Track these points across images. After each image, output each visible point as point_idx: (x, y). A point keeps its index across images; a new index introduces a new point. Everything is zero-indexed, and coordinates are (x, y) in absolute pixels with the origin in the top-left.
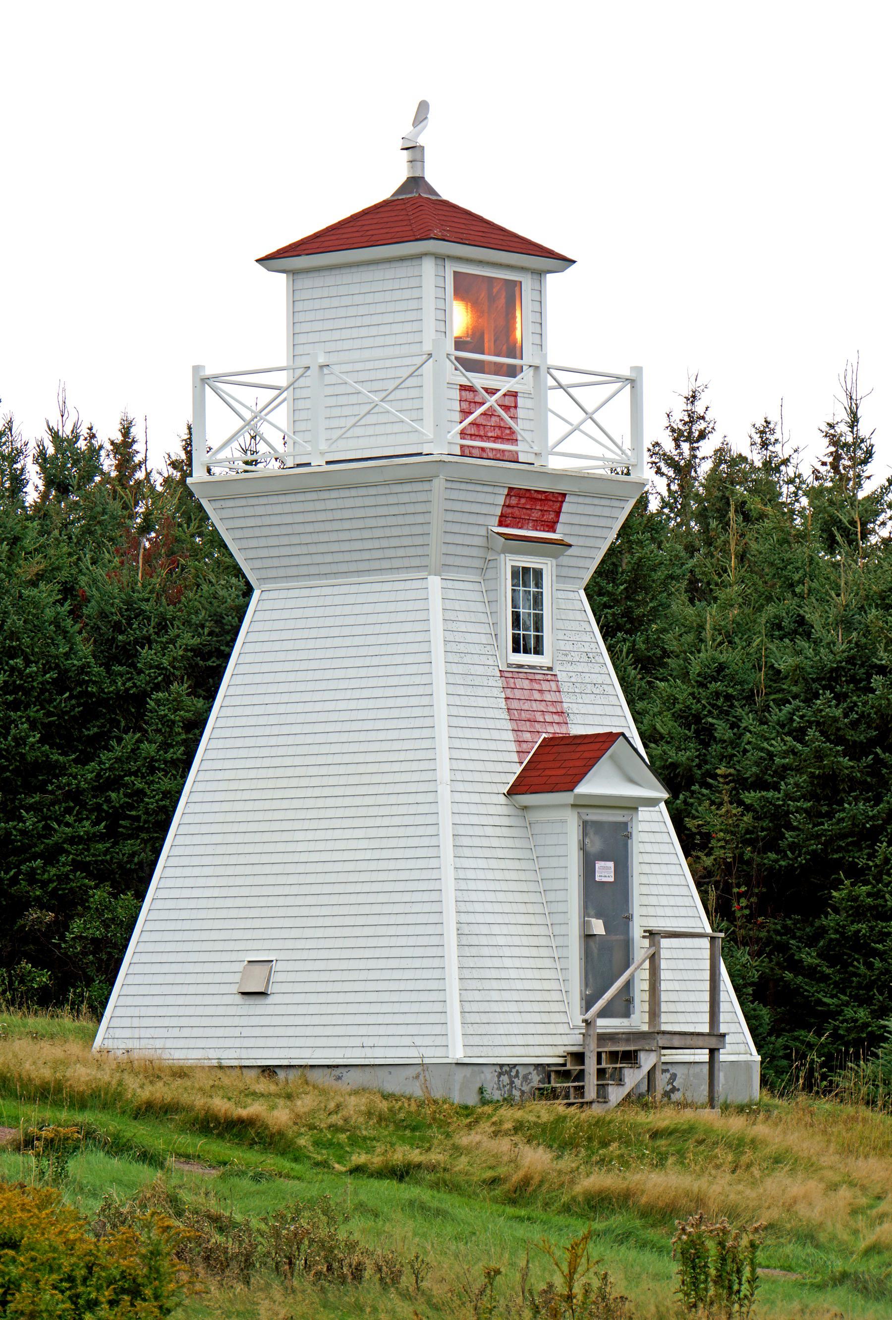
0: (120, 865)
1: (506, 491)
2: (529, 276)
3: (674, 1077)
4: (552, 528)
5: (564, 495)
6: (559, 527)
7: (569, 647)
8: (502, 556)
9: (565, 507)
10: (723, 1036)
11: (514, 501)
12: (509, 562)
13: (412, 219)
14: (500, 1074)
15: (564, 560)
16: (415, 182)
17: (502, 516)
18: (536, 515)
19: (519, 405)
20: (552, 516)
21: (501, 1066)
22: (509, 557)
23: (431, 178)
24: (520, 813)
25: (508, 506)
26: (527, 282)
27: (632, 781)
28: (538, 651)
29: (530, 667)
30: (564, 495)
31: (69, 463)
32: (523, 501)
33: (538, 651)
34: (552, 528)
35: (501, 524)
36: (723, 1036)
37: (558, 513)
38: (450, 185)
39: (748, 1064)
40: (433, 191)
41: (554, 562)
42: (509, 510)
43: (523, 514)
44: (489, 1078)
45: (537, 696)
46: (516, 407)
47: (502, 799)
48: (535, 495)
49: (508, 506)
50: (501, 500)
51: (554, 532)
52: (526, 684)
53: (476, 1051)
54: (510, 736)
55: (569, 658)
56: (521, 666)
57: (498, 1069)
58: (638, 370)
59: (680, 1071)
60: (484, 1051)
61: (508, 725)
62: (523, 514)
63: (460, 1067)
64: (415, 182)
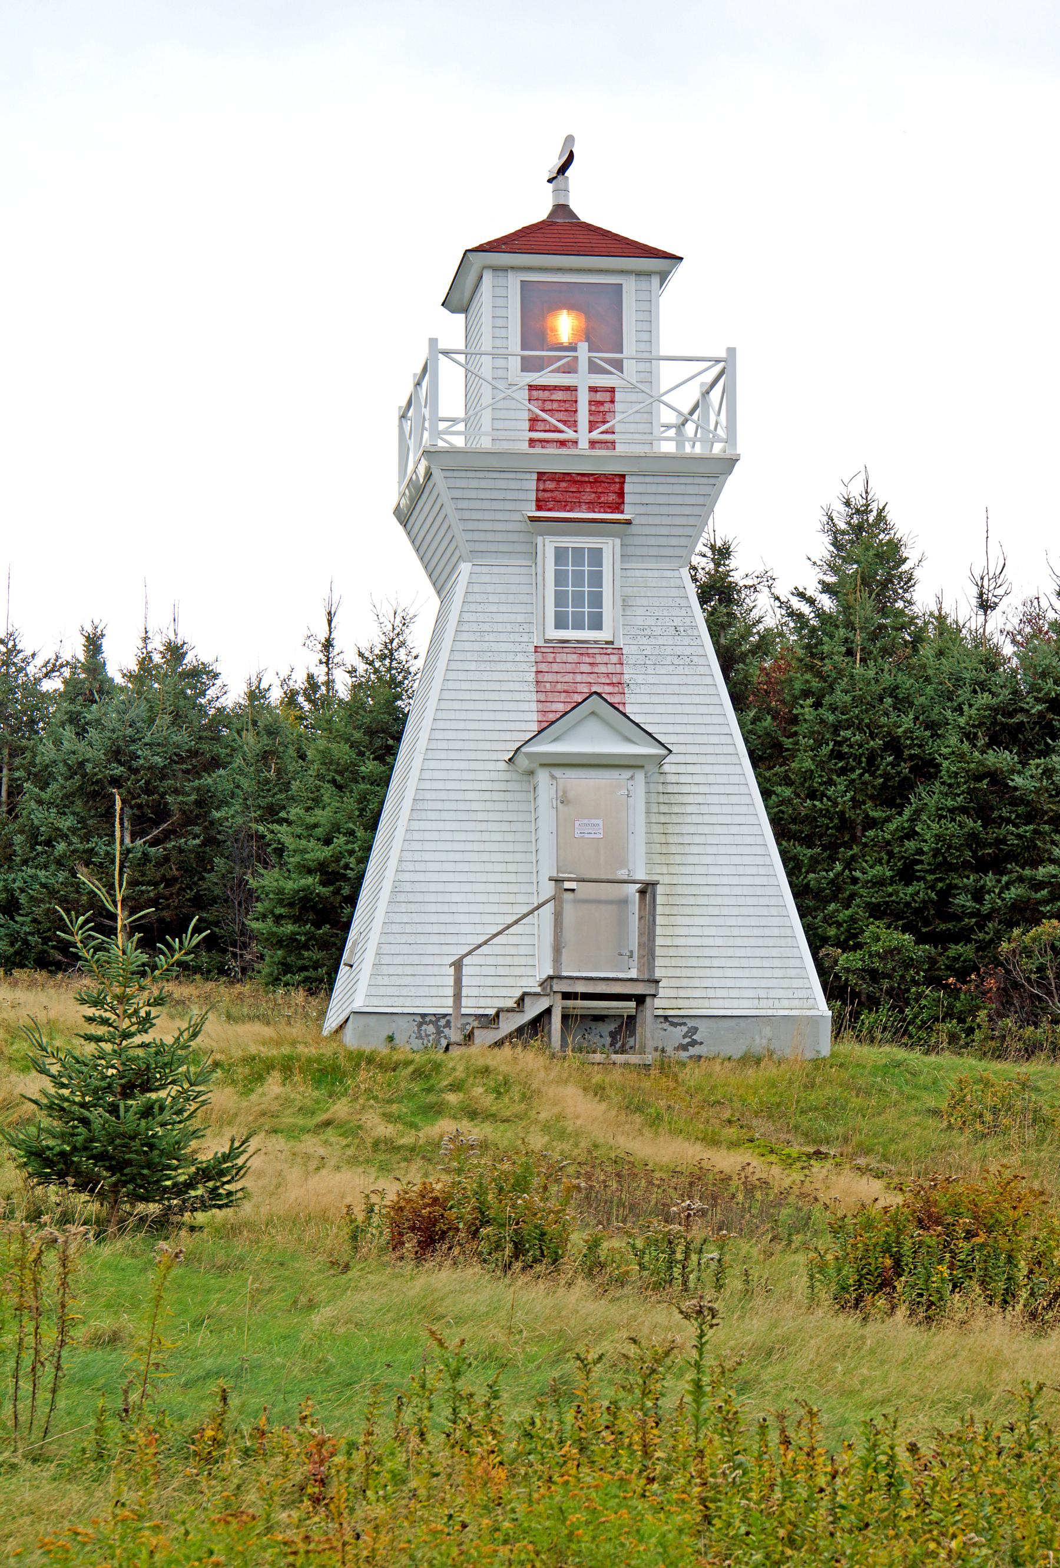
0: (908, 905)
1: (535, 476)
2: (633, 278)
3: (694, 1030)
4: (618, 507)
5: (623, 476)
6: (627, 508)
7: (651, 621)
8: (540, 539)
9: (627, 488)
10: (657, 982)
11: (550, 485)
12: (548, 546)
13: (561, 235)
14: (420, 1025)
15: (629, 540)
16: (561, 209)
17: (538, 500)
18: (587, 497)
19: (617, 398)
20: (612, 497)
21: (423, 1016)
22: (548, 539)
23: (574, 207)
24: (525, 778)
25: (544, 491)
26: (630, 286)
27: (628, 740)
28: (597, 624)
29: (578, 642)
30: (623, 476)
31: (895, 546)
32: (563, 484)
33: (597, 624)
34: (618, 507)
35: (539, 508)
36: (657, 982)
37: (621, 494)
38: (589, 211)
39: (813, 1021)
40: (573, 215)
41: (618, 541)
42: (547, 495)
43: (568, 497)
44: (404, 1031)
45: (586, 668)
46: (612, 401)
47: (503, 766)
48: (579, 478)
49: (544, 491)
50: (533, 485)
51: (622, 512)
52: (573, 658)
53: (375, 1001)
54: (534, 706)
55: (648, 632)
56: (567, 641)
57: (419, 1019)
58: (732, 351)
59: (701, 1025)
60: (399, 1001)
61: (534, 697)
62: (568, 497)
63: (358, 1016)
64: (561, 209)
